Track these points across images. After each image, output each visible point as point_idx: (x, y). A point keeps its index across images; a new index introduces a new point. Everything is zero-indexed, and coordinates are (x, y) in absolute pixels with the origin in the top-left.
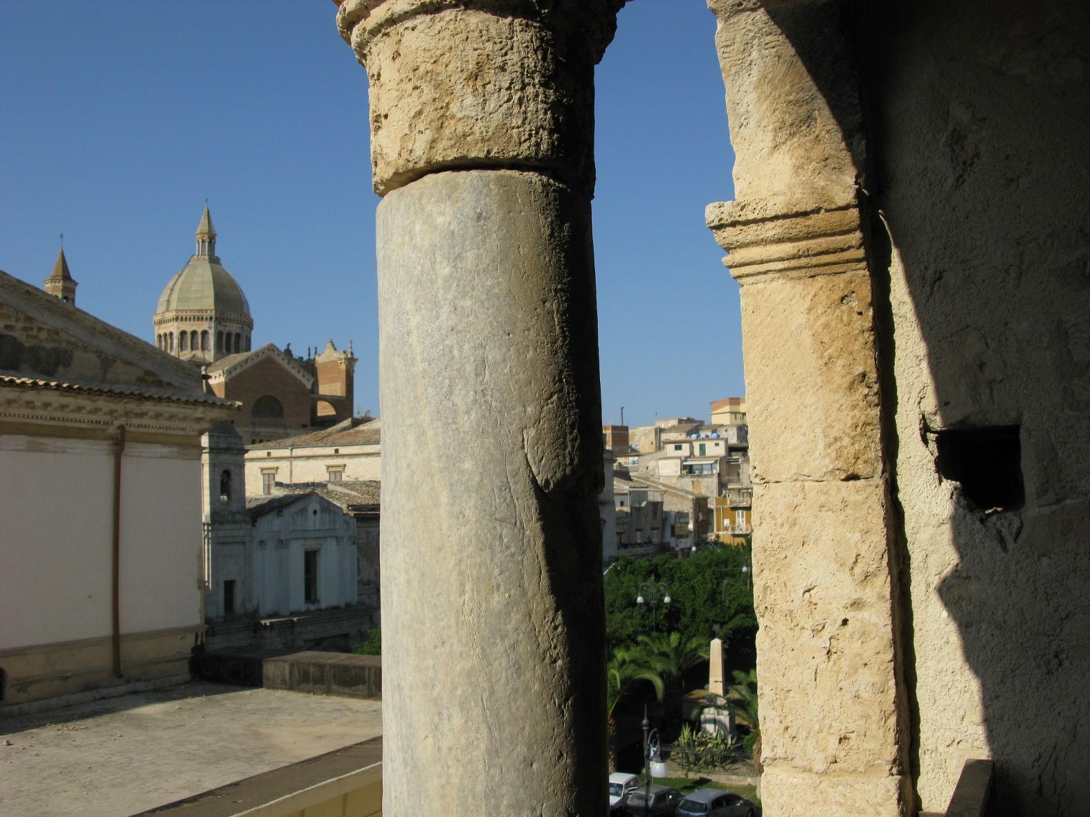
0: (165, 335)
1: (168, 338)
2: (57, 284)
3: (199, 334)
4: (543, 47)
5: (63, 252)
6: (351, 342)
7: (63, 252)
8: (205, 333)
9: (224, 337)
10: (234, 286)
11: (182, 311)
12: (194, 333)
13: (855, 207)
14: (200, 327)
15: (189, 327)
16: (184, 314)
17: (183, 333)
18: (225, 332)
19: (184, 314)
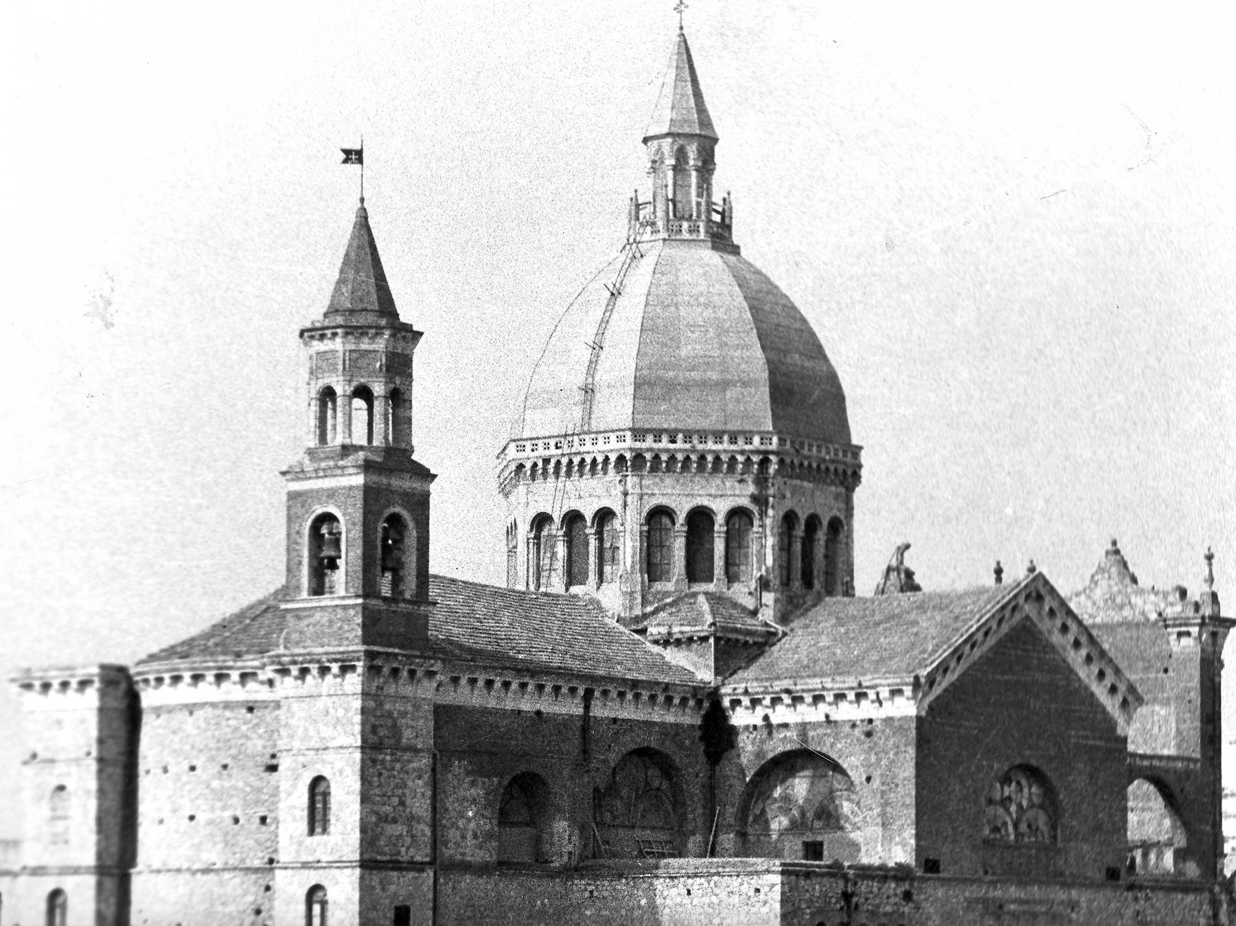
0: (813, 522)
1: (821, 536)
2: (365, 345)
3: (720, 519)
4: (1198, 865)
5: (363, 223)
6: (1210, 558)
7: (363, 223)
8: (604, 515)
9: (800, 531)
10: (772, 289)
11: (658, 434)
12: (700, 519)
13: (87, 870)
14: (589, 496)
15: (680, 497)
16: (664, 443)
17: (658, 516)
18: (803, 516)
19: (664, 443)
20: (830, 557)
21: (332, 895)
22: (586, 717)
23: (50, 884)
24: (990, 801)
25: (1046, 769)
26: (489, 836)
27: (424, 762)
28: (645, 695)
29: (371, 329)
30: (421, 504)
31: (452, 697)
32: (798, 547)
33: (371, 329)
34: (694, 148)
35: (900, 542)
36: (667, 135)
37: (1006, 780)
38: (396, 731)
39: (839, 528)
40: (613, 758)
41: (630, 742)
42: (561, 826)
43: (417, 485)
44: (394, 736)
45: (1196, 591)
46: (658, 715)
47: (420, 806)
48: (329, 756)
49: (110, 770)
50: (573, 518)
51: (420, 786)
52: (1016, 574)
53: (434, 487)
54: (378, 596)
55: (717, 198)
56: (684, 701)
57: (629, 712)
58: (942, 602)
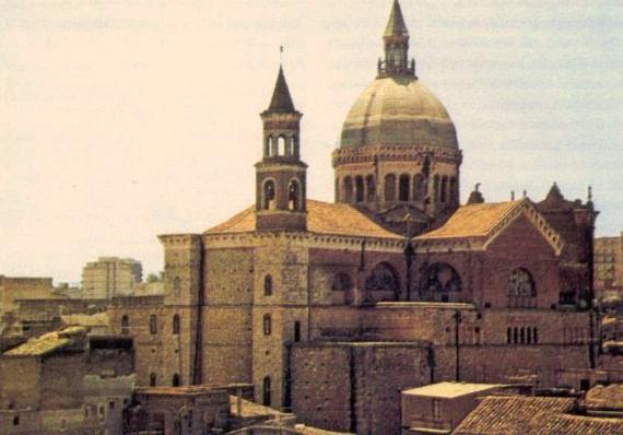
1: (448, 184)
5: (281, 71)
7: (281, 71)
9: (440, 183)
17: (390, 177)
20: (452, 192)
21: (274, 317)
22: (363, 251)
23: (174, 312)
24: (509, 281)
25: (529, 269)
26: (329, 294)
27: (305, 268)
28: (390, 243)
29: (282, 113)
30: (303, 176)
31: (314, 245)
32: (440, 187)
33: (282, 113)
34: (398, 40)
35: (475, 183)
36: (280, 306)
37: (514, 273)
38: (295, 259)
39: (455, 181)
40: (374, 265)
41: (379, 260)
42: (355, 290)
43: (302, 169)
44: (310, 342)
45: (584, 202)
46: (390, 250)
47: (304, 284)
48: (272, 267)
49: (100, 276)
50: (359, 180)
51: (303, 277)
52: (519, 197)
53: (308, 170)
54: (288, 209)
55: (410, 59)
56: (398, 245)
57: (378, 249)
58: (494, 206)
